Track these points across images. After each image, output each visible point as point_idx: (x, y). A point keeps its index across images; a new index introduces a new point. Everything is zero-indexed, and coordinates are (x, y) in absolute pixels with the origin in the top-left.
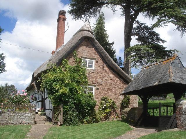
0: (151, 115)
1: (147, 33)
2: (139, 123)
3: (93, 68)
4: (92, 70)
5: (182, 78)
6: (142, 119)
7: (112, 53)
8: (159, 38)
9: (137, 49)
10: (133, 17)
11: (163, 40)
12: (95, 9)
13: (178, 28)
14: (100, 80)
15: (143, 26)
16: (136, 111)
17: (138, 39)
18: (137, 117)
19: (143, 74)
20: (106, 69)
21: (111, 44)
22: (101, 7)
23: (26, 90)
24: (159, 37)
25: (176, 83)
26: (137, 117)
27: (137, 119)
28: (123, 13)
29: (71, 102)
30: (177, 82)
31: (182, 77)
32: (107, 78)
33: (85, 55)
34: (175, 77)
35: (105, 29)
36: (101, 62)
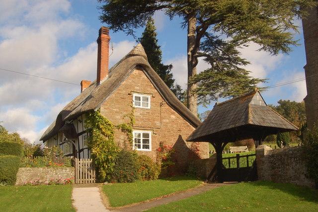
0: (227, 167)
1: (220, 50)
2: (211, 179)
3: (149, 108)
4: (147, 109)
5: (263, 119)
6: (214, 174)
7: (170, 82)
8: (238, 58)
9: (206, 75)
10: (201, 30)
11: (245, 61)
12: (142, 15)
13: (264, 48)
14: (158, 123)
15: (215, 40)
16: (208, 163)
17: (207, 60)
18: (209, 171)
19: (216, 114)
20: (166, 107)
21: (167, 67)
22: (152, 13)
23: (40, 140)
24: (238, 56)
25: (255, 125)
26: (209, 171)
27: (208, 173)
28: (185, 21)
29: (170, 125)
30: (257, 124)
31: (264, 117)
32: (167, 121)
33: (136, 89)
34: (254, 118)
35: (158, 44)
36: (159, 99)
